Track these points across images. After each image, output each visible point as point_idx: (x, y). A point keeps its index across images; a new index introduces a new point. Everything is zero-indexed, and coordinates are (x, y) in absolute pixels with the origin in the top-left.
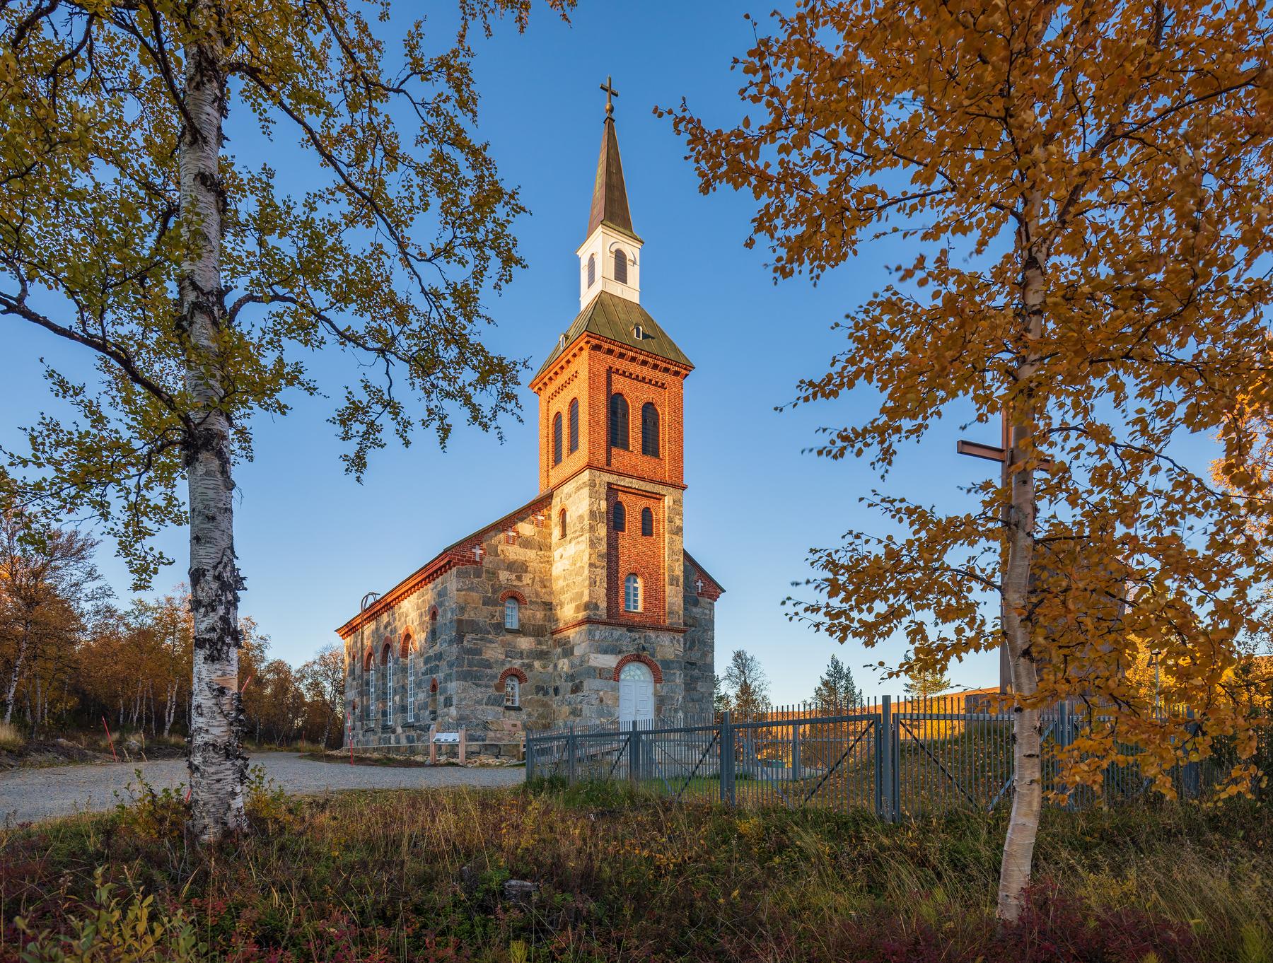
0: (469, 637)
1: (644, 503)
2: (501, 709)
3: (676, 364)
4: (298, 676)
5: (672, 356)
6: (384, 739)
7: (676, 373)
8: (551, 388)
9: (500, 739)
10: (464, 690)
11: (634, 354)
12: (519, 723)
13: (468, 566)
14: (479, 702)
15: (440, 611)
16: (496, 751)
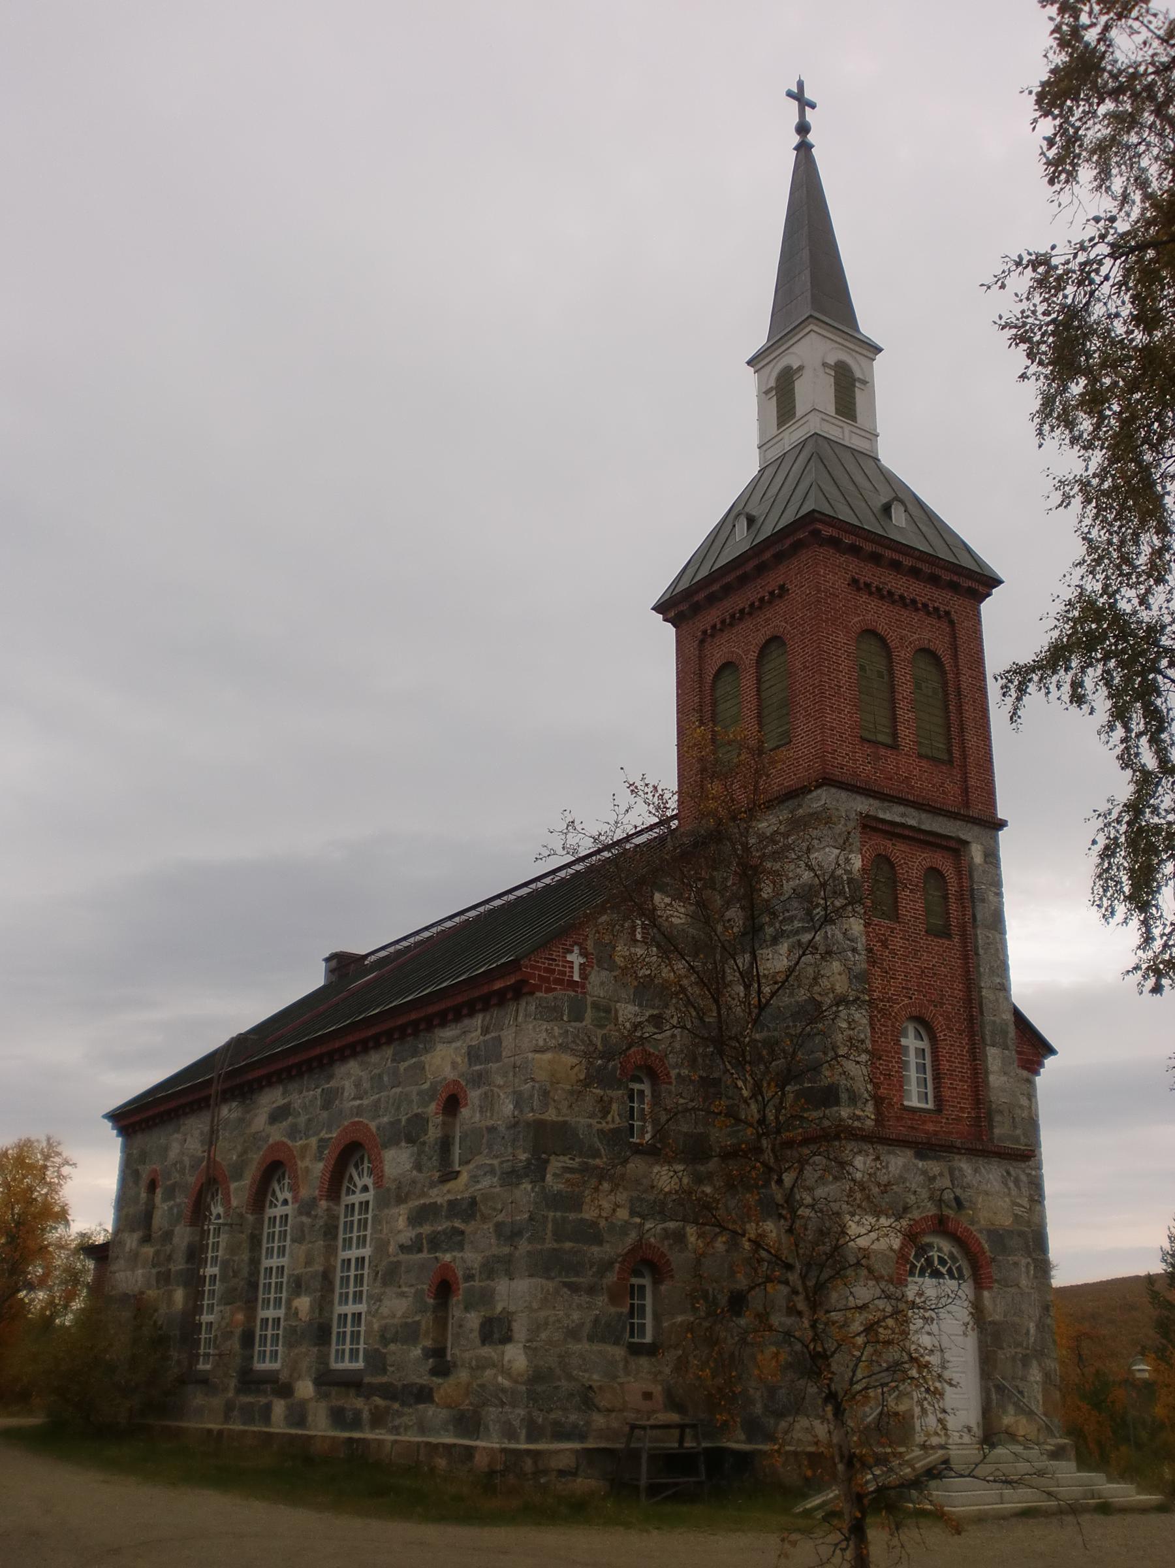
0: (556, 1164)
2: (618, 1352)
4: (701, 1305)
8: (712, 616)
12: (657, 1390)
13: (560, 992)
14: (573, 1334)
15: (474, 1095)
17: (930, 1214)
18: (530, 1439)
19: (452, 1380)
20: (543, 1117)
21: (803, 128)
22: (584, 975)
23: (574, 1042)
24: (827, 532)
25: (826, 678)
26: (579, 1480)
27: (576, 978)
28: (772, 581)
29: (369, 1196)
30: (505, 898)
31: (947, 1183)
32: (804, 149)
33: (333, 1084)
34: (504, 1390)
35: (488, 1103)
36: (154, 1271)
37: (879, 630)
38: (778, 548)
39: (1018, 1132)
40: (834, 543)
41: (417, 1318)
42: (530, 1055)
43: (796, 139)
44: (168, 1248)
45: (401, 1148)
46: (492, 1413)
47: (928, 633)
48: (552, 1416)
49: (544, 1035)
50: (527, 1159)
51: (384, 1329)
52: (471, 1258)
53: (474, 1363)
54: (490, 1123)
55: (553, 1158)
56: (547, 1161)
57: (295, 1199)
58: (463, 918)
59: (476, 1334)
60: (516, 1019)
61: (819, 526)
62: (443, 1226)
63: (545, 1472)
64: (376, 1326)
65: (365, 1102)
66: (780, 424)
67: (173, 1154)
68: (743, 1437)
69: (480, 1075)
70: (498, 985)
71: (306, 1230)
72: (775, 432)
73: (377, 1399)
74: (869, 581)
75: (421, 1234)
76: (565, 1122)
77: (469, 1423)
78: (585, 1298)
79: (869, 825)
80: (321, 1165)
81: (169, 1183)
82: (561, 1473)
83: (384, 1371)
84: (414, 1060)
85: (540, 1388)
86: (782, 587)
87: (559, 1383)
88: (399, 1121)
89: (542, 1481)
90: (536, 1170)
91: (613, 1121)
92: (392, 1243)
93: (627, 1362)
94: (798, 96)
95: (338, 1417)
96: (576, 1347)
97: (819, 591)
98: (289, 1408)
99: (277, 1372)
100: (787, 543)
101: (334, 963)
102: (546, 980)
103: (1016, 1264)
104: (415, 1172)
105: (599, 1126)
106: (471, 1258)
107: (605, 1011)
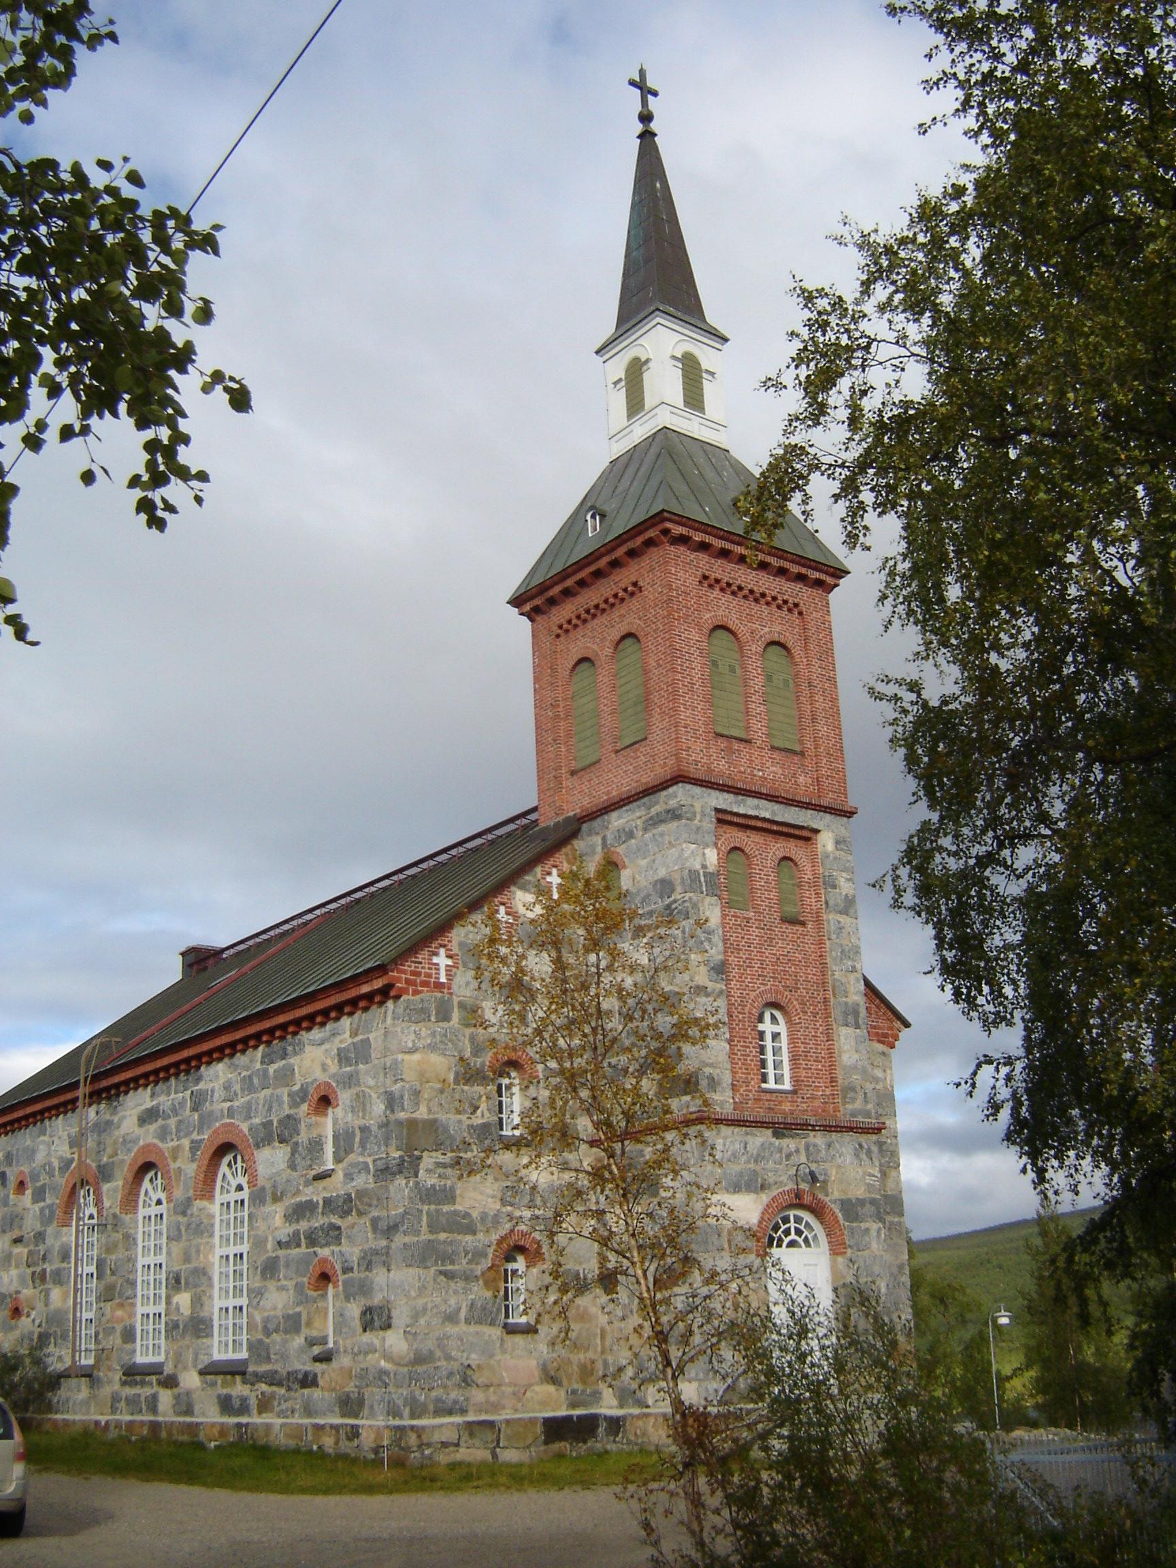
0: (428, 1160)
1: (779, 848)
3: (816, 566)
5: (811, 552)
6: (133, 1402)
7: (819, 583)
8: (566, 611)
9: (496, 1407)
10: (422, 1289)
11: (761, 557)
13: (426, 994)
14: (451, 1318)
15: (344, 1097)
16: (490, 1436)
17: (786, 1189)
18: (413, 1416)
19: (335, 1364)
20: (414, 1115)
21: (646, 118)
22: (450, 976)
23: (441, 1042)
24: (678, 530)
25: (679, 676)
26: (461, 1450)
27: (443, 979)
28: (623, 578)
29: (245, 1195)
30: (367, 890)
31: (803, 1159)
32: (647, 137)
33: (201, 1086)
34: (387, 1373)
35: (361, 1103)
36: (29, 1271)
37: (731, 625)
38: (630, 545)
39: (870, 1106)
40: (683, 540)
41: (298, 1309)
42: (400, 1057)
43: (639, 127)
44: (42, 1248)
45: (274, 1148)
46: (374, 1394)
47: (774, 625)
48: (433, 1394)
49: (413, 1037)
50: (401, 1157)
51: (266, 1321)
52: (351, 1251)
53: (356, 1350)
54: (361, 1122)
55: (425, 1154)
56: (420, 1158)
57: (169, 1200)
58: (324, 910)
59: (357, 1322)
60: (384, 1021)
61: (668, 525)
62: (319, 1221)
63: (429, 1445)
64: (258, 1318)
65: (236, 1104)
66: (630, 416)
67: (40, 1157)
68: (615, 1402)
69: (351, 1076)
70: (365, 989)
71: (183, 1230)
72: (626, 424)
73: (263, 1385)
74: (719, 577)
75: (298, 1231)
76: (435, 1121)
77: (350, 1405)
78: (461, 1284)
79: (724, 819)
80: (194, 1166)
81: (39, 1184)
82: (445, 1445)
83: (268, 1360)
84: (284, 1062)
85: (420, 1369)
86: (635, 584)
87: (438, 1364)
88: (271, 1122)
89: (426, 1452)
90: (409, 1166)
91: (483, 1116)
92: (270, 1238)
93: (502, 1340)
94: (640, 85)
95: (226, 1405)
96: (451, 1330)
97: (671, 589)
98: (177, 1397)
99: (161, 1365)
100: (639, 541)
101: (192, 958)
102: (414, 983)
103: (867, 1230)
104: (289, 1171)
105: (469, 1122)
106: (351, 1251)
107: (472, 1014)
